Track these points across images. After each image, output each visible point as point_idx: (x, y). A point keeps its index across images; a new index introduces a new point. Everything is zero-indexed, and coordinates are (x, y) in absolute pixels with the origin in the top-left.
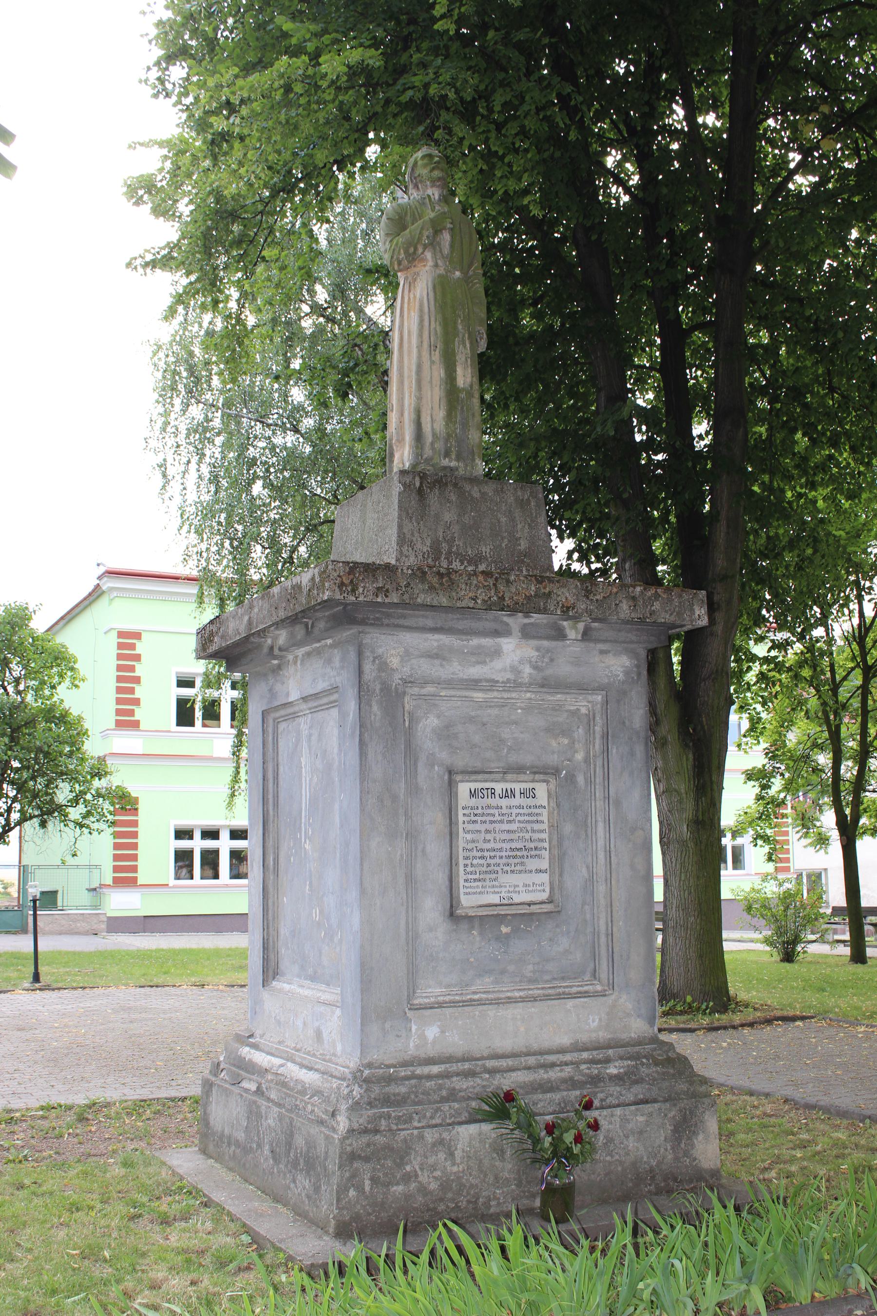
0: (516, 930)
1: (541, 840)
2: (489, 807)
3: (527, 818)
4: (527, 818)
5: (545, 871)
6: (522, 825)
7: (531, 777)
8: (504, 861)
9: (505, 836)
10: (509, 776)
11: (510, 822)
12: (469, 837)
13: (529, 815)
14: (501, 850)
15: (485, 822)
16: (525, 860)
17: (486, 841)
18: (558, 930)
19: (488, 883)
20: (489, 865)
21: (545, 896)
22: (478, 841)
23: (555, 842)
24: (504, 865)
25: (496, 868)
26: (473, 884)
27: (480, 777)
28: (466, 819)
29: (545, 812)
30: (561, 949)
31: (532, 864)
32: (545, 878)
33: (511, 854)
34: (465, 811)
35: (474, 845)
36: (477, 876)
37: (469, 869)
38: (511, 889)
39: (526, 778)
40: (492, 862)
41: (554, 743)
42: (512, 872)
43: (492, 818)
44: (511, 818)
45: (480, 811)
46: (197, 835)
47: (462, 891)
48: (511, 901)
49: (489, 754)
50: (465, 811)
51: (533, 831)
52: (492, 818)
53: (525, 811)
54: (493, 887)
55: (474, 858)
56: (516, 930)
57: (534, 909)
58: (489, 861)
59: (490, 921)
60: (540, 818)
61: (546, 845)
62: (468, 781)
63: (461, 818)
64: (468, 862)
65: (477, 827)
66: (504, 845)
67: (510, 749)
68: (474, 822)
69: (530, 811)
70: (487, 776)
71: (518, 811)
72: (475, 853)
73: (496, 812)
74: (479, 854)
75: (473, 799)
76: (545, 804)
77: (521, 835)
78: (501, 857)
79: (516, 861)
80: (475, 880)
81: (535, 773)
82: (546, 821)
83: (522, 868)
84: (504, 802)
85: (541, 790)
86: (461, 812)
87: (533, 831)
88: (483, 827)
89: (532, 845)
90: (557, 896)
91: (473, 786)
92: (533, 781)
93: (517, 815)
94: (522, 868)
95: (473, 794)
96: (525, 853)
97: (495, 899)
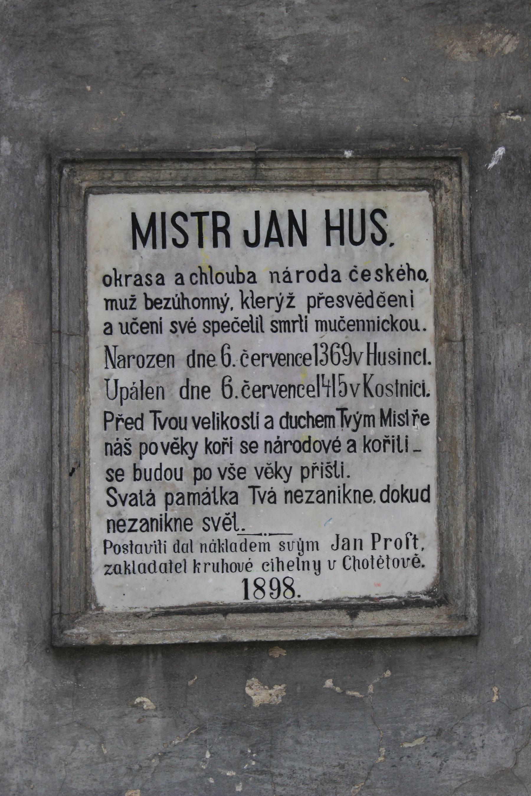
0: (302, 698)
1: (411, 389)
2: (204, 276)
3: (351, 313)
4: (351, 313)
5: (422, 496)
6: (331, 337)
7: (365, 171)
8: (261, 458)
9: (261, 375)
10: (279, 170)
11: (283, 326)
12: (127, 377)
13: (360, 301)
14: (249, 421)
15: (189, 327)
16: (343, 457)
17: (189, 391)
18: (469, 700)
19: (197, 534)
20: (201, 474)
21: (419, 580)
22: (161, 393)
23: (455, 397)
24: (263, 472)
25: (228, 485)
26: (139, 538)
27: (166, 173)
28: (117, 317)
29: (424, 294)
30: (481, 765)
31: (370, 471)
32: (423, 518)
33: (286, 435)
34: (115, 292)
35: (146, 405)
36: (156, 511)
37: (126, 486)
38: (288, 556)
39: (345, 174)
40: (215, 461)
41: (461, 53)
42: (294, 496)
43: (215, 315)
44: (287, 314)
45: (169, 290)
46: (167, 326)
47: (98, 559)
48: (285, 597)
49: (204, 96)
50: (115, 292)
51: (376, 357)
52: (215, 315)
53: (345, 288)
54: (220, 546)
55: (148, 448)
56: (302, 698)
57: (369, 624)
58: (202, 459)
59: (198, 661)
60: (402, 313)
61: (427, 405)
62: (122, 189)
63: (97, 315)
64: (125, 462)
65: (160, 343)
66: (262, 407)
67: (287, 76)
68: (151, 327)
69: (364, 288)
70: (191, 170)
71: (317, 288)
72: (149, 432)
73: (233, 291)
74: (166, 436)
75: (146, 252)
76: (424, 261)
77: (329, 370)
78: (249, 447)
79: (307, 459)
80: (148, 524)
81: (378, 157)
82: (427, 321)
83: (333, 484)
84: (264, 260)
85: (411, 222)
86: (97, 295)
87: (376, 357)
88: (180, 346)
89: (372, 406)
90: (463, 581)
91: (145, 204)
92: (375, 186)
93: (314, 302)
94: (333, 484)
95: (144, 233)
96: (344, 434)
97: (227, 589)
